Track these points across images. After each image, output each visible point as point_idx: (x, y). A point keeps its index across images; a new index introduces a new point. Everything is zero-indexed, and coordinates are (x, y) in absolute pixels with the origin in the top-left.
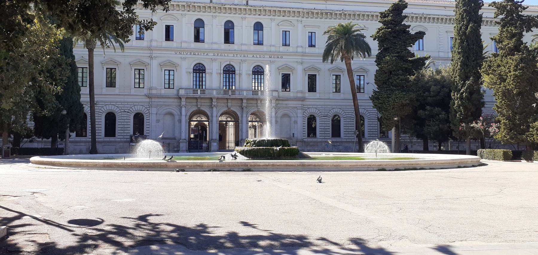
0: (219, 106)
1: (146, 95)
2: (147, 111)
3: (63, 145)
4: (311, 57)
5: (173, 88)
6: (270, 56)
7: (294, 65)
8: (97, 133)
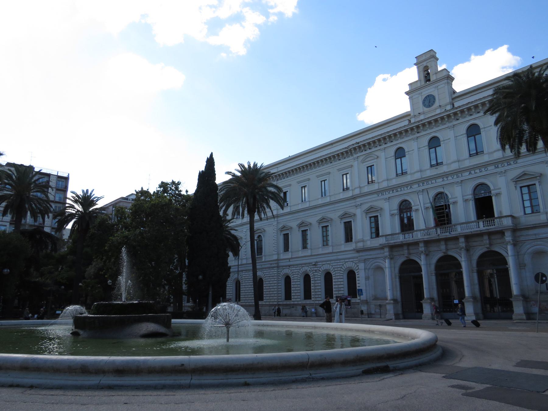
0: (432, 252)
1: (354, 250)
2: (356, 267)
3: (294, 308)
4: (364, 197)
5: (372, 237)
6: (496, 166)
7: (352, 211)
8: (293, 297)
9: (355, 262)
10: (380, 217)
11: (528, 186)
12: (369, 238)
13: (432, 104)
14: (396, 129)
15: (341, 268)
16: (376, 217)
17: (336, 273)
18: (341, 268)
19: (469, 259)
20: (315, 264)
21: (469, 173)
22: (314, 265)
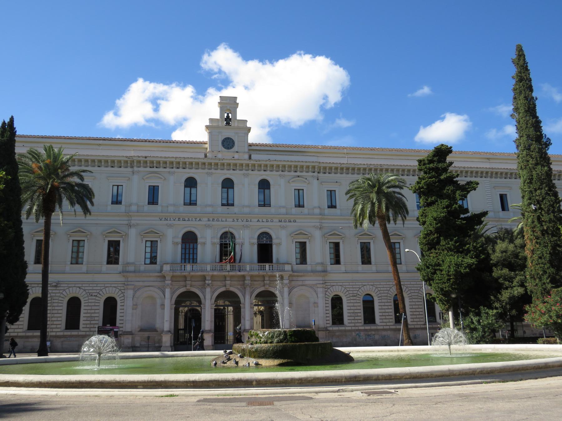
9: (119, 288)
10: (160, 242)
11: (152, 241)
12: (69, 263)
13: (231, 147)
14: (194, 158)
15: (62, 293)
16: (117, 243)
17: (89, 299)
18: (62, 293)
19: (172, 293)
20: (56, 285)
21: (257, 220)
22: (56, 286)
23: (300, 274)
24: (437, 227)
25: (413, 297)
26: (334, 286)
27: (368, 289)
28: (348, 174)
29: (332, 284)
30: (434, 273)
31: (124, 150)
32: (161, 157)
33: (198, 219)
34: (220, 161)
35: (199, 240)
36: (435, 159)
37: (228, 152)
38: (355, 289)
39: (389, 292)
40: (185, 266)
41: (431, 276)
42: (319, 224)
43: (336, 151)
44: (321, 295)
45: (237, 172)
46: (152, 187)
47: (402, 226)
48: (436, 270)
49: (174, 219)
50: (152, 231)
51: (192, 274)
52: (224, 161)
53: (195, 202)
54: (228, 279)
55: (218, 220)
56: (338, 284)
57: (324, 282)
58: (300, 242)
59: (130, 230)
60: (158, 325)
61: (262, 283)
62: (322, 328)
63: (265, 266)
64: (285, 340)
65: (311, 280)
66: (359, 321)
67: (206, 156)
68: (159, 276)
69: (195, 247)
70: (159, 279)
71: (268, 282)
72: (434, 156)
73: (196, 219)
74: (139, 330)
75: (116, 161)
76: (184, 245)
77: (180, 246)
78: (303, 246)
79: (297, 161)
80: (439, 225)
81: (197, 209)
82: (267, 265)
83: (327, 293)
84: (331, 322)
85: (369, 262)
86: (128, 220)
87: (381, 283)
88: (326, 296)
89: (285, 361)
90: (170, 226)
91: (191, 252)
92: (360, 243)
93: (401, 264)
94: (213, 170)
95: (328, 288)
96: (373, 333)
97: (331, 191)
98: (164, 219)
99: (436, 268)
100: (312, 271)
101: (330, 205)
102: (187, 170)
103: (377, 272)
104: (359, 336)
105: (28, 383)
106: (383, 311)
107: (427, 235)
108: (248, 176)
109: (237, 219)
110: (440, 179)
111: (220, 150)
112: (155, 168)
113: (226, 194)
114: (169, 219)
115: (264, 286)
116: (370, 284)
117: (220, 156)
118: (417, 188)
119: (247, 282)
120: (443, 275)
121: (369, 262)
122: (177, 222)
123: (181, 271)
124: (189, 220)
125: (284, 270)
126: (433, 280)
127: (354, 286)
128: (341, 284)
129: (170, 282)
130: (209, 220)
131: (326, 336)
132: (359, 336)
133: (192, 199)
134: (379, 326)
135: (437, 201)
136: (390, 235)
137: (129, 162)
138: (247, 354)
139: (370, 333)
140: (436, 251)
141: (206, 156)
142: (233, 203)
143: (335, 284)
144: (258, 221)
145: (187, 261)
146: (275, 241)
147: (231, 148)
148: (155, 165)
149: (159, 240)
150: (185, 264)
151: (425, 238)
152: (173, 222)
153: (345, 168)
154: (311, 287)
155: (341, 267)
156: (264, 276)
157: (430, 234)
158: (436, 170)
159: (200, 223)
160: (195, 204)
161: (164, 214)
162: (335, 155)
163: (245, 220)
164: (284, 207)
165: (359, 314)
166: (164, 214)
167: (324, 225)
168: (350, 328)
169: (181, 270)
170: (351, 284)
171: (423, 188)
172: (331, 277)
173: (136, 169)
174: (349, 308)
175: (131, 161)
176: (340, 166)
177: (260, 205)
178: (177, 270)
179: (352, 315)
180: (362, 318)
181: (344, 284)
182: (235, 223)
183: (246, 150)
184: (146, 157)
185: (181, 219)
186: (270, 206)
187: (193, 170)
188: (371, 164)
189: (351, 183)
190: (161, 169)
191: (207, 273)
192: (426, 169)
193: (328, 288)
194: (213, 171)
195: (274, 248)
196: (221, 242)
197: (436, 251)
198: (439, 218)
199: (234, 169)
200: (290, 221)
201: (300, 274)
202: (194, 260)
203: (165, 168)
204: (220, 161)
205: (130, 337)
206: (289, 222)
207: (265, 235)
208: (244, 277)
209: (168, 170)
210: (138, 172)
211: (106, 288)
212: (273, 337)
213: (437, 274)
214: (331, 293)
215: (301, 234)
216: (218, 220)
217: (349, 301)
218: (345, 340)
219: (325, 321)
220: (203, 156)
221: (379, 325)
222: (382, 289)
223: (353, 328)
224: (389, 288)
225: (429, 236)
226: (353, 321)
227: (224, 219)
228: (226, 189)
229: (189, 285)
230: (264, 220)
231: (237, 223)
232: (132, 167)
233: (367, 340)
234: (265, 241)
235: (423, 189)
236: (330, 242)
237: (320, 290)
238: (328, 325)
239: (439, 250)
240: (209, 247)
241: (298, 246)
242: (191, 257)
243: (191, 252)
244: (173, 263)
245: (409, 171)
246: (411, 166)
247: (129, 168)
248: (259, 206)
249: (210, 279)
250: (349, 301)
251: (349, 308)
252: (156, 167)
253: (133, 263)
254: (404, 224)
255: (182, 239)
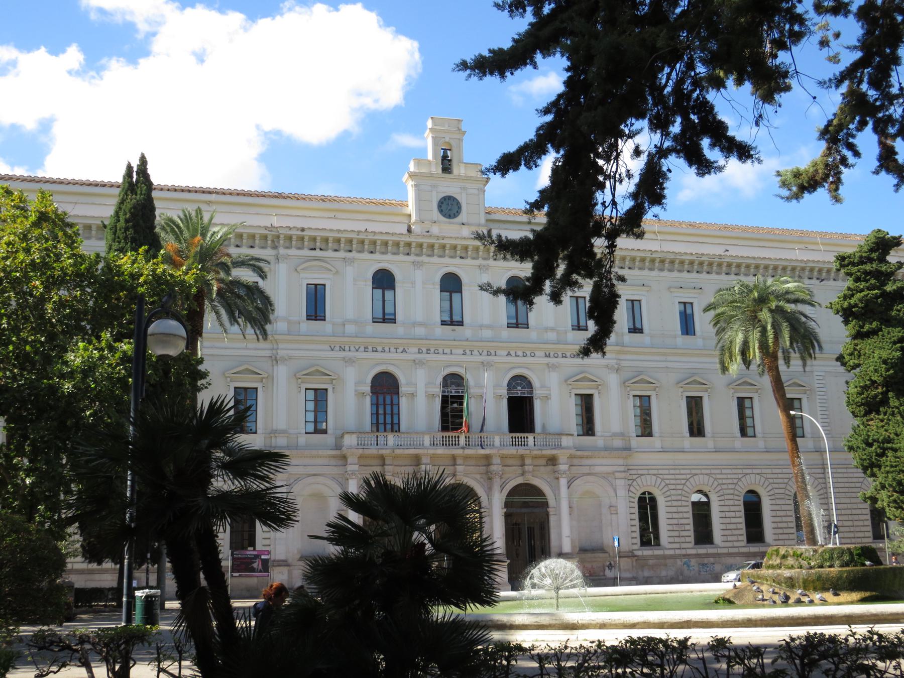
11: (316, 390)
14: (393, 234)
21: (506, 353)
23: (586, 453)
24: (889, 375)
25: (778, 496)
26: (643, 475)
27: (701, 481)
28: (661, 270)
29: (640, 472)
30: (883, 455)
31: (257, 214)
32: (331, 230)
33: (401, 349)
34: (438, 241)
35: (403, 389)
36: (874, 255)
37: (450, 223)
38: (679, 482)
39: (737, 487)
40: (377, 437)
41: (876, 459)
42: (615, 361)
43: (380, 208)
44: (622, 492)
45: (469, 261)
46: (313, 286)
47: (801, 369)
48: (885, 449)
49: (357, 348)
50: (318, 371)
51: (398, 452)
52: (445, 242)
53: (393, 317)
54: (459, 461)
55: (436, 351)
56: (651, 472)
57: (626, 468)
58: (581, 395)
59: (275, 367)
60: (606, 541)
61: (519, 470)
62: (625, 552)
63: (458, 437)
64: (851, 562)
65: (604, 464)
66: (688, 539)
67: (409, 231)
68: (334, 457)
69: (395, 402)
70: (333, 462)
71: (531, 468)
72: (872, 250)
73: (396, 349)
74: (298, 557)
75: (245, 236)
76: (374, 398)
77: (368, 400)
78: (586, 403)
79: (384, 232)
80: (891, 372)
81: (397, 329)
82: (531, 437)
83: (632, 489)
84: (638, 541)
85: (650, 435)
86: (272, 349)
87: (724, 471)
88: (631, 494)
89: (868, 594)
90: (349, 361)
91: (388, 410)
92: (738, 398)
93: (803, 437)
94: (424, 256)
95: (634, 480)
96: (712, 560)
97: (633, 301)
98: (337, 348)
99: (886, 445)
100: (606, 449)
101: (632, 327)
102: (377, 256)
103: (835, 451)
104: (688, 566)
105: (728, 621)
106: (728, 520)
107: (865, 388)
108: (487, 269)
109: (396, 349)
110: (885, 291)
111: (435, 219)
112: (318, 250)
113: (449, 302)
114: (347, 348)
115: (523, 474)
116: (755, 471)
117: (435, 230)
118: (845, 307)
119: (493, 468)
120: (898, 458)
121: (650, 435)
122: (361, 355)
123: (377, 447)
124: (383, 351)
125: (559, 447)
126: (879, 467)
127: (677, 477)
128: (655, 472)
129: (356, 467)
130: (420, 352)
131: (633, 566)
132: (688, 566)
133: (387, 311)
134: (720, 547)
135: (881, 330)
136: (785, 385)
137: (270, 238)
138: (799, 586)
139: (706, 561)
140: (881, 417)
141: (409, 231)
142: (461, 320)
143: (645, 472)
144: (509, 354)
145: (381, 427)
146: (538, 392)
147: (455, 216)
148: (318, 244)
149: (259, 386)
150: (378, 434)
151: (860, 394)
152: (357, 354)
153: (658, 260)
154: (605, 476)
155: (655, 442)
156: (522, 457)
157: (869, 388)
158: (877, 274)
159: (404, 356)
160: (394, 321)
161: (561, 346)
162: (696, 239)
163: (485, 353)
164: (552, 329)
165: (687, 527)
166: (346, 339)
167: (624, 363)
168: (671, 552)
169: (377, 444)
170: (672, 472)
171: (857, 307)
172: (640, 459)
173: (282, 251)
174: (670, 516)
175: (273, 236)
176: (650, 255)
177: (510, 326)
178: (371, 444)
179: (675, 528)
180: (692, 533)
181: (660, 472)
182: (468, 358)
183: (483, 221)
184: (303, 230)
185: (370, 348)
186: (528, 328)
187: (389, 257)
188: (703, 254)
189: (718, 292)
190: (330, 254)
191: (426, 451)
192: (859, 274)
193: (634, 480)
194: (424, 259)
195: (537, 405)
196: (443, 392)
197: (881, 417)
198: (892, 359)
199: (463, 255)
200: (374, 349)
201: (586, 453)
202: (395, 427)
203: (336, 250)
204: (438, 241)
205: (285, 570)
206: (563, 357)
207: (519, 380)
208: (488, 458)
209: (342, 254)
210: (287, 257)
211: (642, 477)
212: (833, 558)
213: (887, 457)
214: (638, 488)
215: (642, 381)
216: (436, 351)
217: (669, 504)
218: (664, 573)
219: (630, 539)
220: (405, 231)
221: (721, 546)
222: (724, 481)
223: (678, 552)
224: (685, 481)
225: (867, 391)
226: (677, 540)
227: (447, 351)
228: (448, 294)
229: (389, 474)
230: (520, 353)
231: (472, 357)
232: (275, 247)
233: (702, 573)
234: (519, 392)
235: (856, 309)
236: (634, 396)
237: (620, 483)
238: (635, 547)
239: (885, 414)
240: (555, 404)
241: (579, 402)
242: (389, 420)
243: (388, 410)
244: (359, 432)
245: (633, 259)
246: (770, 259)
247: (269, 248)
248: (373, 322)
249: (428, 461)
250: (669, 504)
251: (670, 516)
252: (321, 249)
253: (284, 432)
254: (804, 365)
255: (372, 387)
